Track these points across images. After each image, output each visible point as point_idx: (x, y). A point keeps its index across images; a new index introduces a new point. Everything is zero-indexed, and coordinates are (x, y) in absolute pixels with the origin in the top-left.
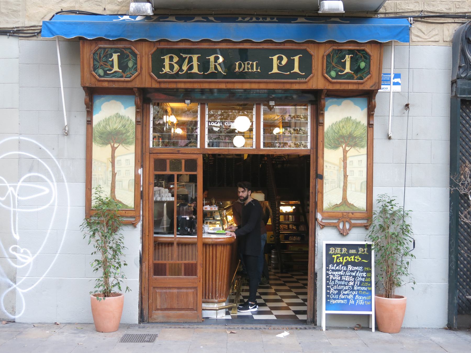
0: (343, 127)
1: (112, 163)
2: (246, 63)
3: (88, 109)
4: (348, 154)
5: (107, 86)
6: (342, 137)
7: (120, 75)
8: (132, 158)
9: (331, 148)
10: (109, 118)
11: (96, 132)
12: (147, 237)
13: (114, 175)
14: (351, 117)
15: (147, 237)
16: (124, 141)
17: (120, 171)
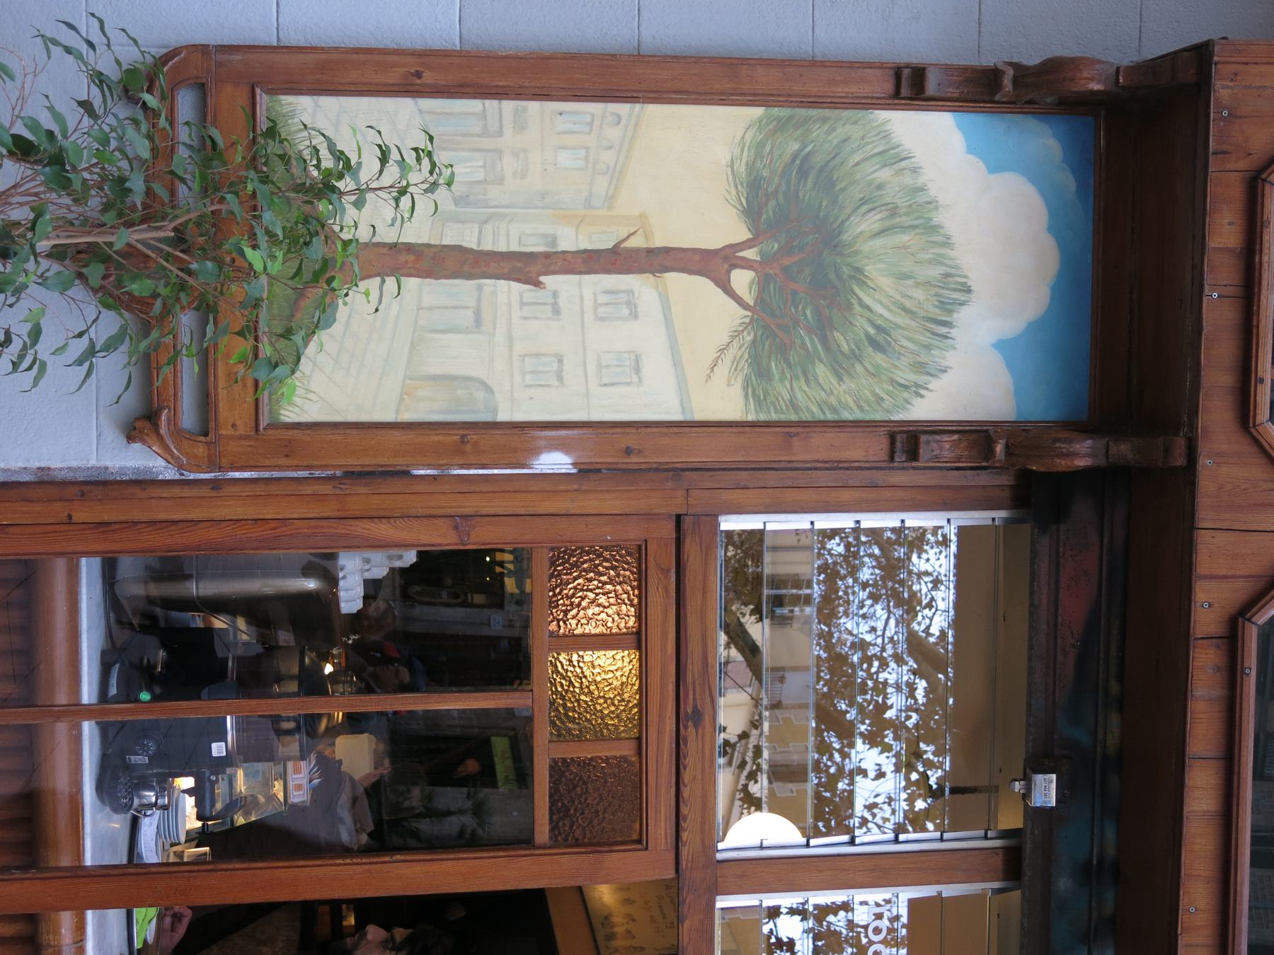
1: (615, 250)
3: (1007, 82)
5: (1214, 242)
8: (653, 399)
10: (934, 229)
11: (841, 132)
12: (60, 511)
13: (525, 267)
15: (60, 511)
16: (773, 336)
17: (556, 311)
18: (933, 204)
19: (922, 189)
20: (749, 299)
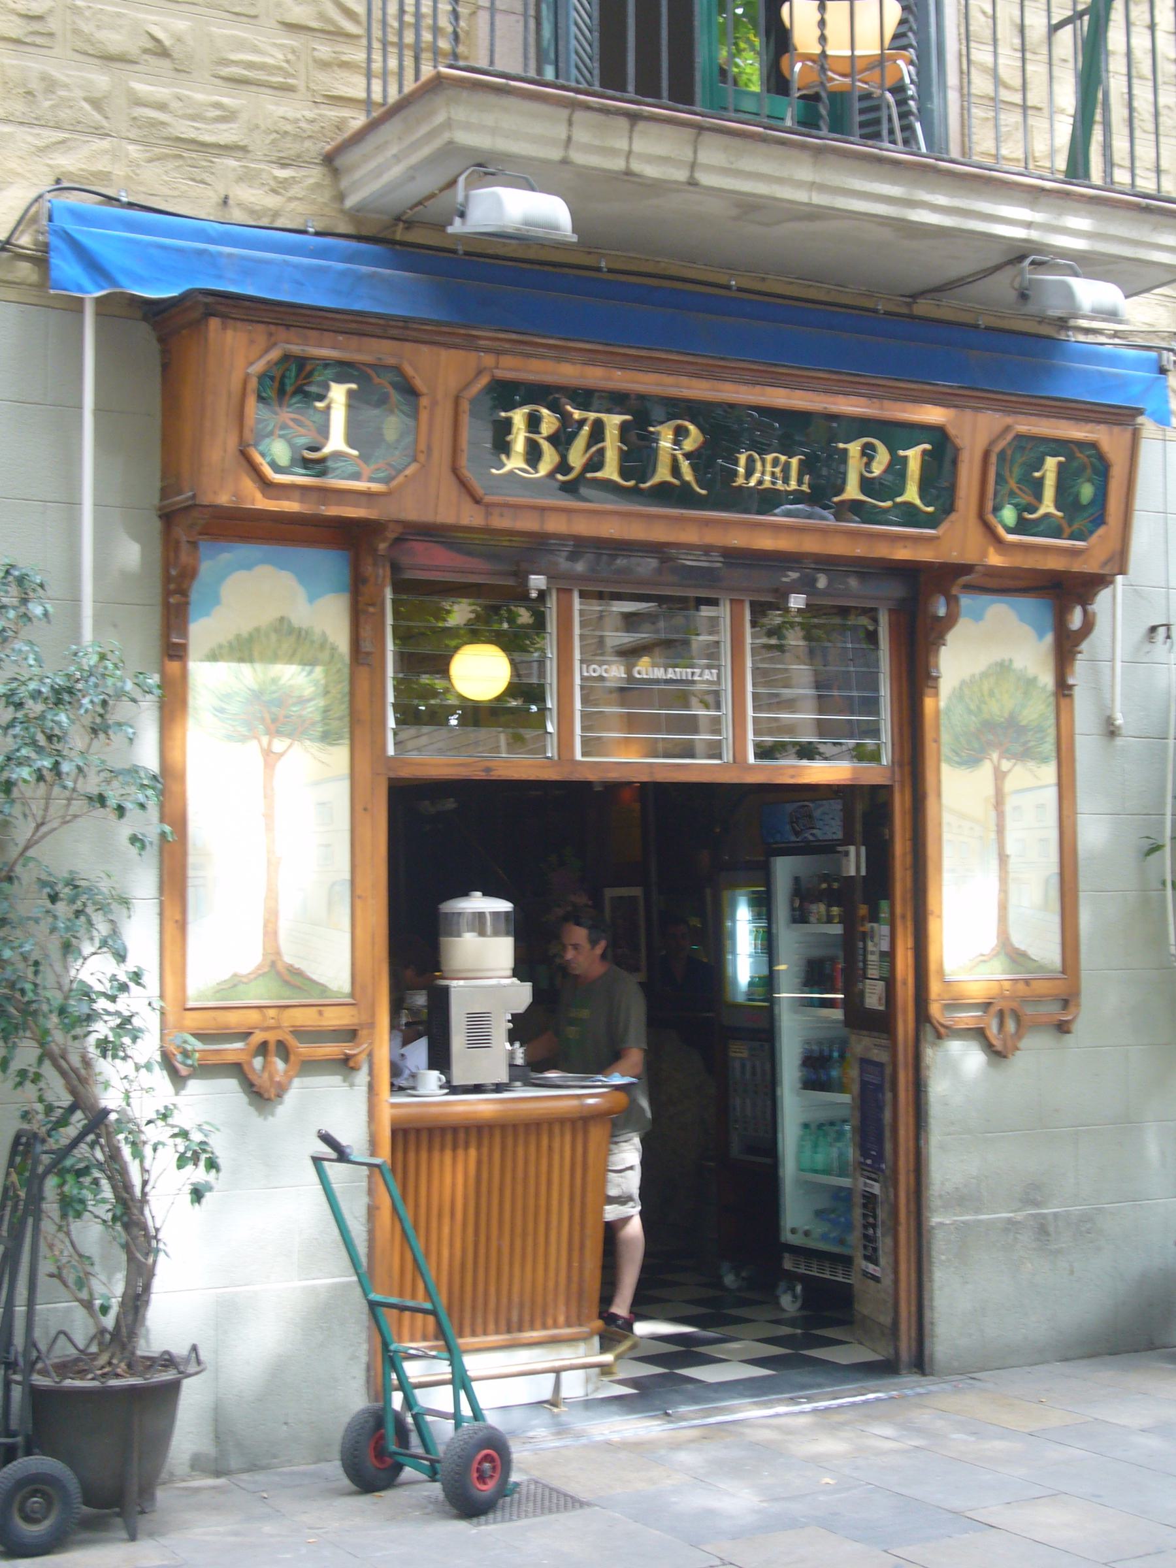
0: (991, 694)
2: (769, 458)
4: (1009, 785)
6: (989, 725)
7: (351, 469)
9: (960, 764)
10: (250, 635)
14: (1011, 660)
18: (238, 636)
19: (230, 643)
20: (288, 741)
